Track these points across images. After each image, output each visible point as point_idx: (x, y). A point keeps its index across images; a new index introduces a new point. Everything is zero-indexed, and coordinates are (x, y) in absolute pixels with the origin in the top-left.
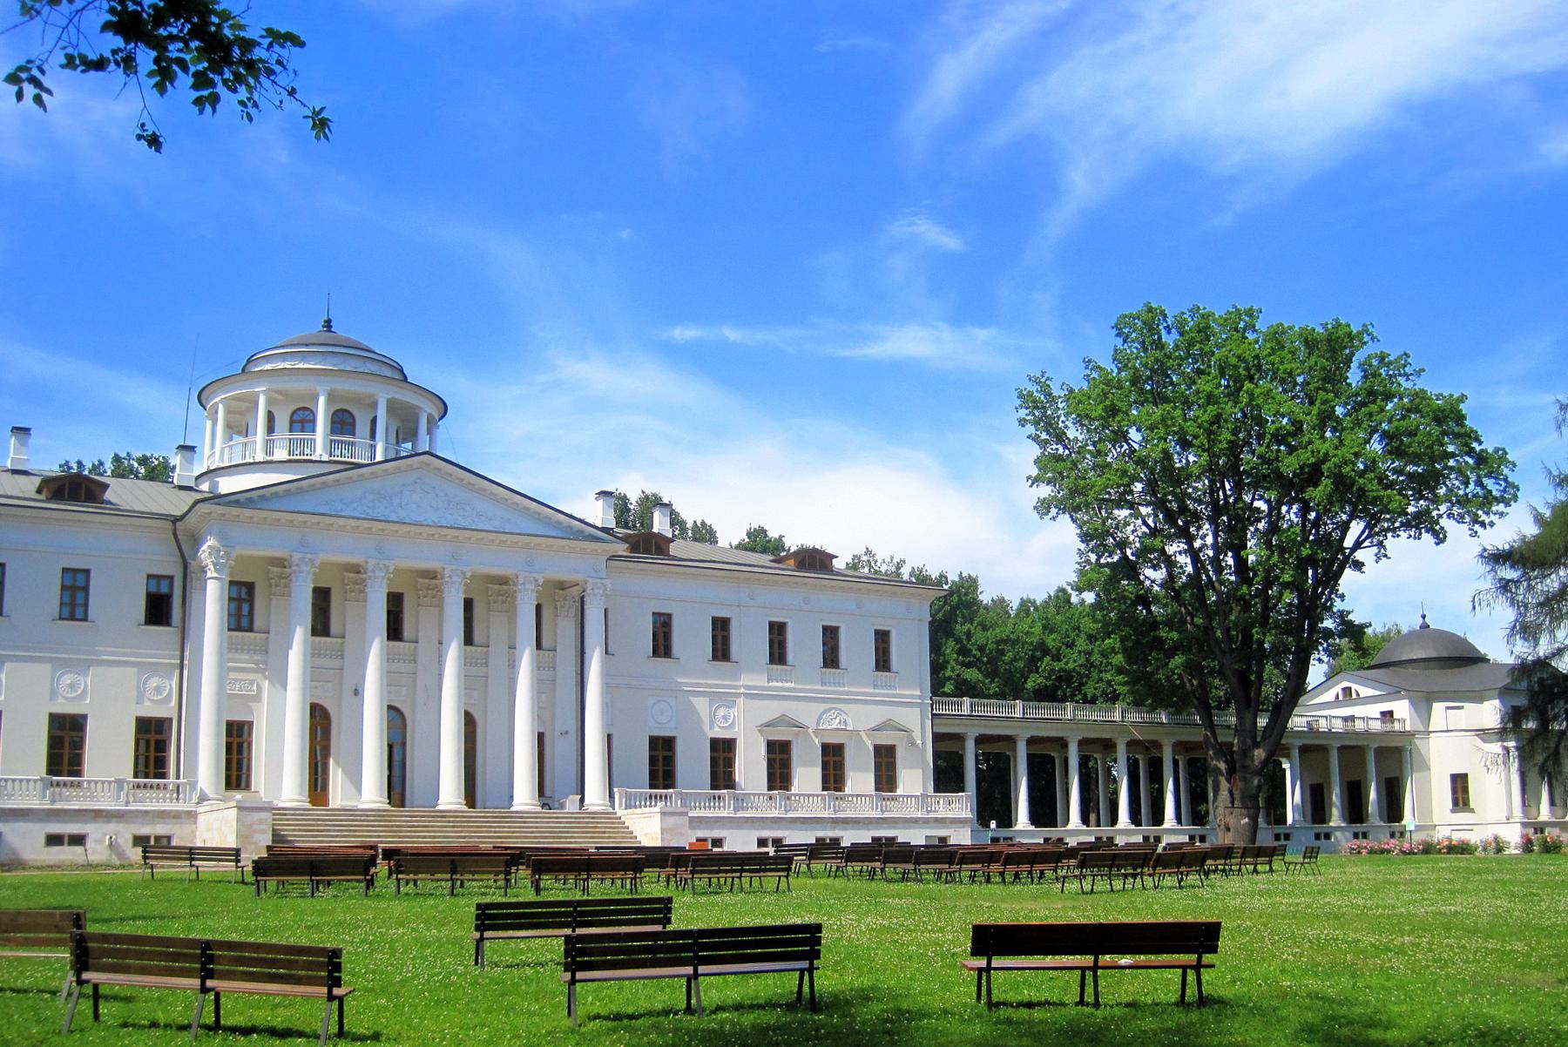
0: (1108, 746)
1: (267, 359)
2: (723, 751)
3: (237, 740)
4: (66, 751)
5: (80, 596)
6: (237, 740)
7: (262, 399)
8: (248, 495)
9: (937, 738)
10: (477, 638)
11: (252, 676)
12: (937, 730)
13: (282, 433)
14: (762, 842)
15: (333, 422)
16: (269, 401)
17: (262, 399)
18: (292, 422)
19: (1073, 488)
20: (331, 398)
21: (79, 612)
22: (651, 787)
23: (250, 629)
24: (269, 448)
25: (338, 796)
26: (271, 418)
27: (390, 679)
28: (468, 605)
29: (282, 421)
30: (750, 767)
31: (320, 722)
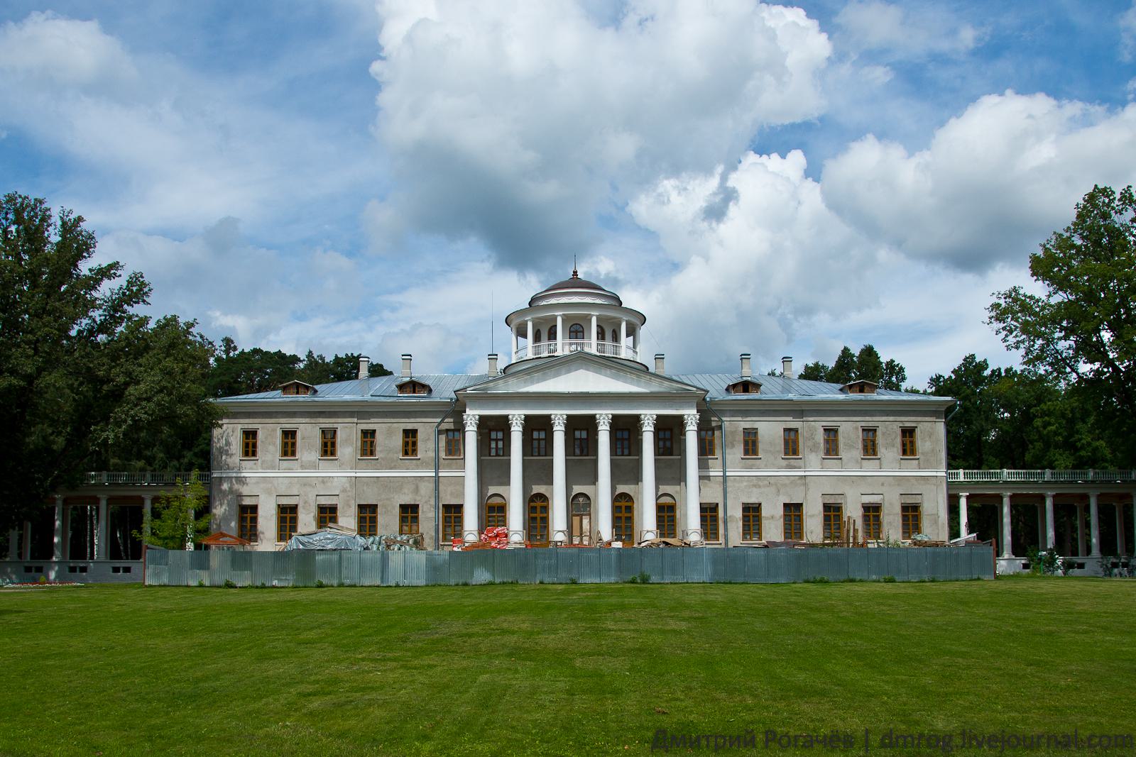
18: (570, 332)
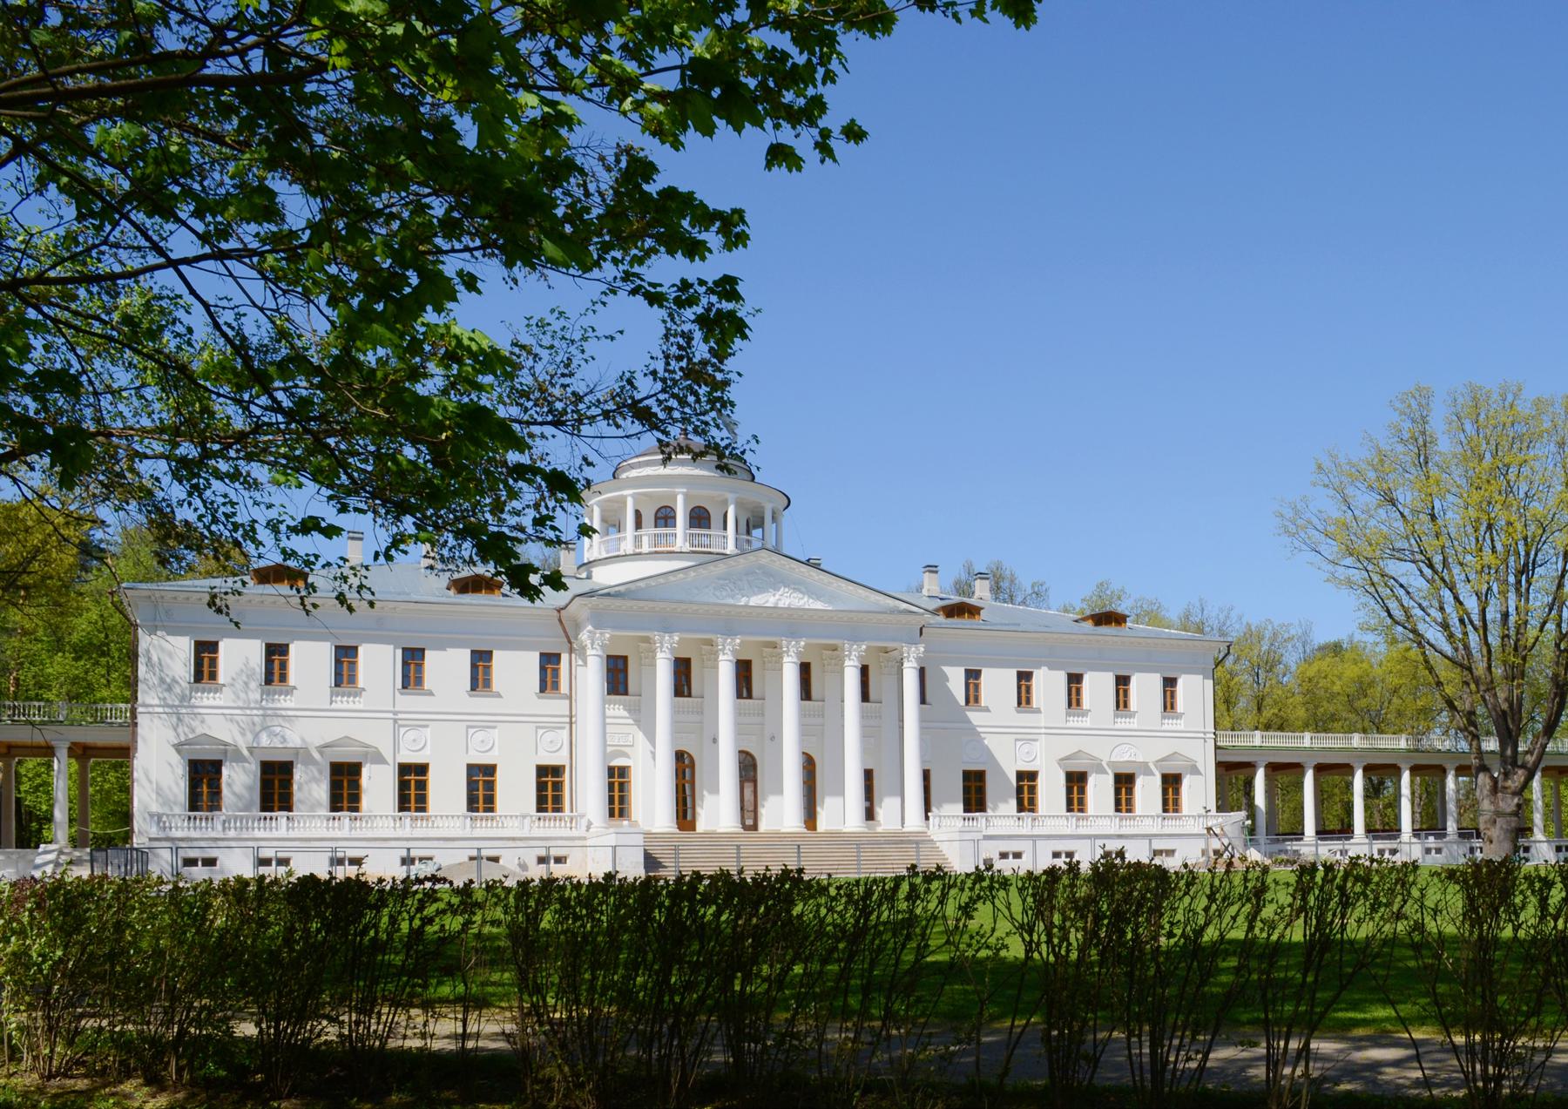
0: (1298, 768)
1: (632, 467)
2: (1027, 779)
3: (618, 783)
4: (550, 793)
5: (621, 676)
6: (618, 783)
7: (630, 502)
8: (642, 584)
9: (1219, 765)
10: (872, 695)
11: (626, 729)
12: (1221, 759)
13: (649, 531)
14: (1056, 855)
15: (691, 518)
16: (635, 502)
17: (630, 502)
18: (657, 518)
19: (1365, 560)
20: (740, 505)
21: (621, 689)
22: (263, 809)
23: (690, 695)
24: (638, 541)
25: (827, 820)
26: (638, 515)
27: (804, 731)
28: (864, 671)
29: (648, 517)
30: (1051, 791)
31: (684, 766)
